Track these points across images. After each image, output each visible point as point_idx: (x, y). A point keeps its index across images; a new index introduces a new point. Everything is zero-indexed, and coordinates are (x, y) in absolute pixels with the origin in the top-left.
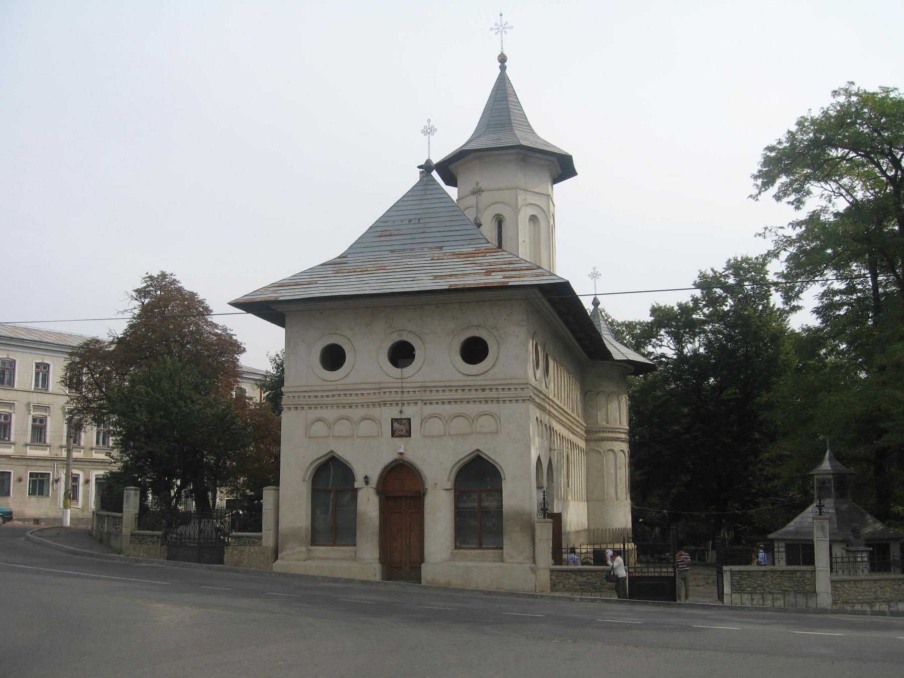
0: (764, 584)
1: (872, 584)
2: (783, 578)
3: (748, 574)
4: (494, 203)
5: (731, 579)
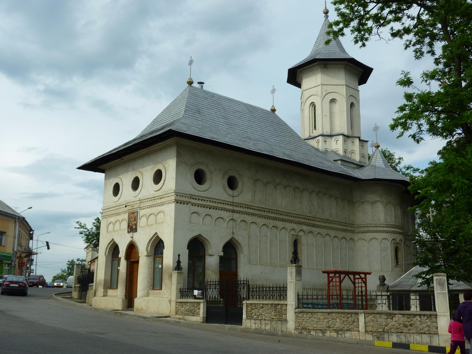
4: (310, 96)
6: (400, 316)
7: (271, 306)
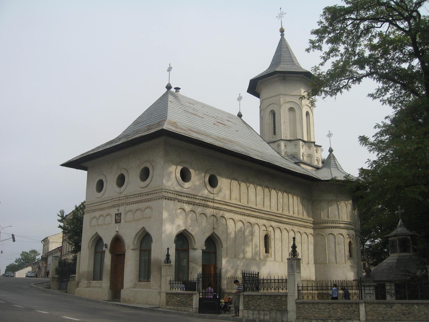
1: (327, 306)
3: (252, 297)
5: (244, 301)
6: (399, 305)
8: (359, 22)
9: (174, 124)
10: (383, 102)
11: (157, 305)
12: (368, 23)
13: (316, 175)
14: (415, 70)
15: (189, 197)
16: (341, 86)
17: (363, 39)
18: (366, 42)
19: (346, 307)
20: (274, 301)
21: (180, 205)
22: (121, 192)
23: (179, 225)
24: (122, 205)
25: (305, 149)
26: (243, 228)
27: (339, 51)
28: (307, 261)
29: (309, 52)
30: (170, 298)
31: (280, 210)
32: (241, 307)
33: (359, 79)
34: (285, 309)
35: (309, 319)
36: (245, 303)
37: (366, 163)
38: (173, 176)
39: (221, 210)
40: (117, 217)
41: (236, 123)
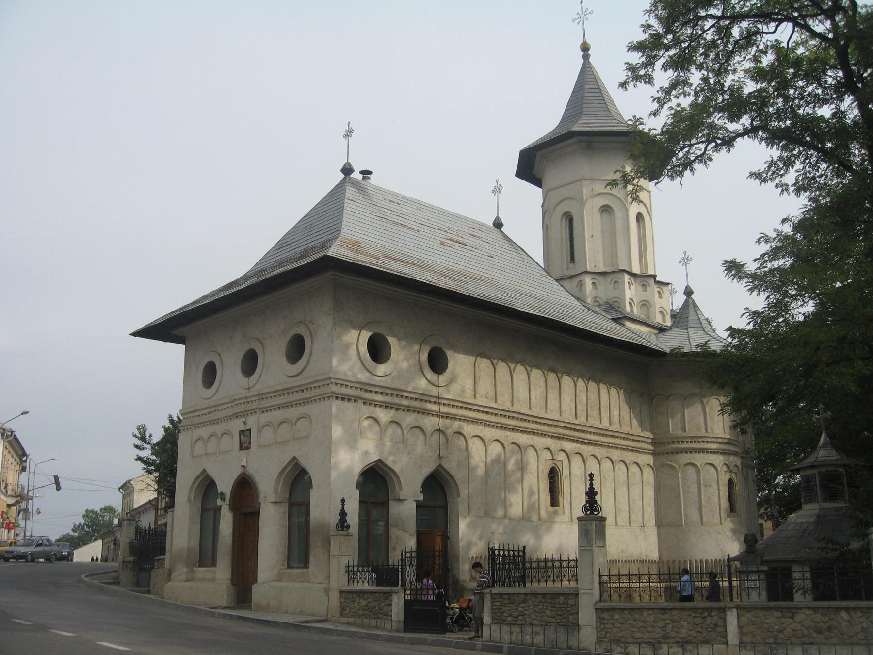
0: (525, 612)
2: (545, 604)
3: (509, 598)
5: (493, 605)
6: (808, 612)
7: (543, 598)
8: (729, 24)
9: (356, 245)
10: (781, 189)
11: (322, 616)
12: (749, 25)
13: (657, 344)
14: (850, 119)
15: (387, 394)
16: (692, 158)
17: (740, 59)
18: (748, 65)
19: (698, 617)
20: (553, 605)
21: (367, 410)
22: (250, 386)
23: (367, 452)
24: (251, 413)
25: (636, 289)
26: (503, 454)
27: (691, 85)
28: (642, 521)
29: (626, 88)
30: (348, 601)
31: (582, 417)
32: (487, 619)
33: (728, 142)
34: (574, 622)
35: (623, 643)
36: (496, 609)
37: (742, 315)
38: (353, 351)
39: (456, 419)
40: (242, 438)
41: (490, 239)
